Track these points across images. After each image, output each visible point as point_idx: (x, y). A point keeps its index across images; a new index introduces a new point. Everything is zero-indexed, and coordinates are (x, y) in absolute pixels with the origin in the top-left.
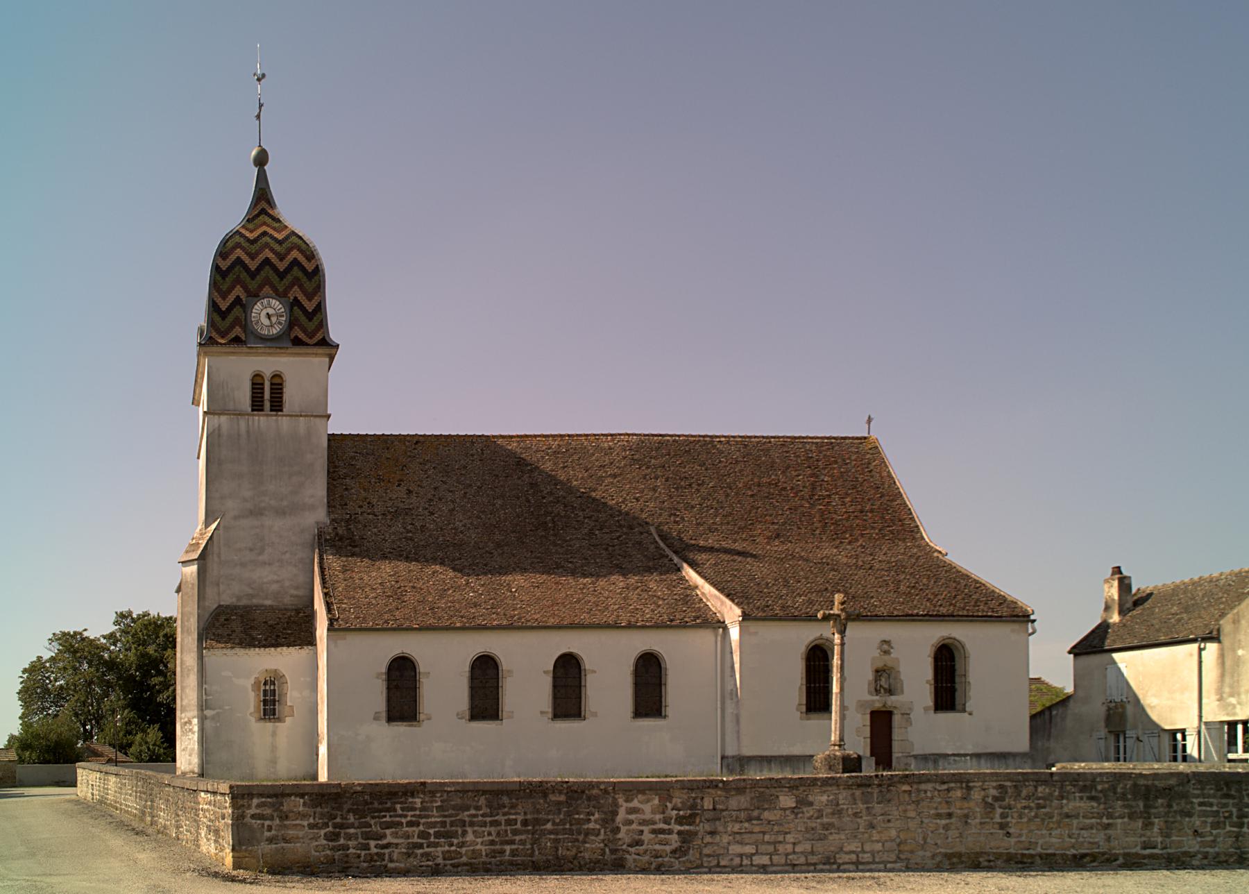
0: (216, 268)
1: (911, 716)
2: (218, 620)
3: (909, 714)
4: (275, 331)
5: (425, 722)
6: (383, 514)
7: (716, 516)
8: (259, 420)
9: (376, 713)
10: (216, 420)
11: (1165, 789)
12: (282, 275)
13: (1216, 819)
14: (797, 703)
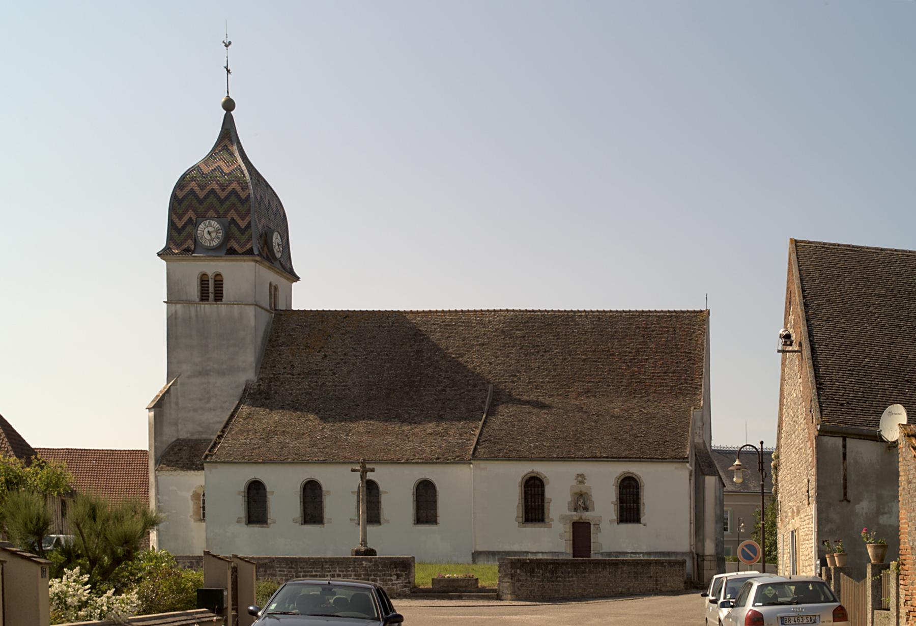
0: (174, 197)
1: (600, 526)
2: (173, 450)
3: (599, 525)
4: (215, 243)
5: (272, 525)
6: (299, 374)
7: (547, 376)
8: (205, 307)
9: (238, 518)
10: (173, 307)
11: (263, 564)
12: (222, 202)
13: (287, 578)
14: (516, 516)
